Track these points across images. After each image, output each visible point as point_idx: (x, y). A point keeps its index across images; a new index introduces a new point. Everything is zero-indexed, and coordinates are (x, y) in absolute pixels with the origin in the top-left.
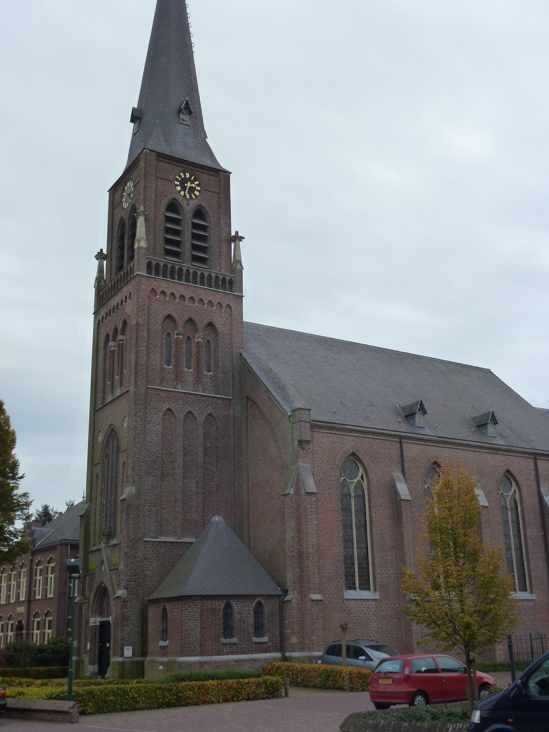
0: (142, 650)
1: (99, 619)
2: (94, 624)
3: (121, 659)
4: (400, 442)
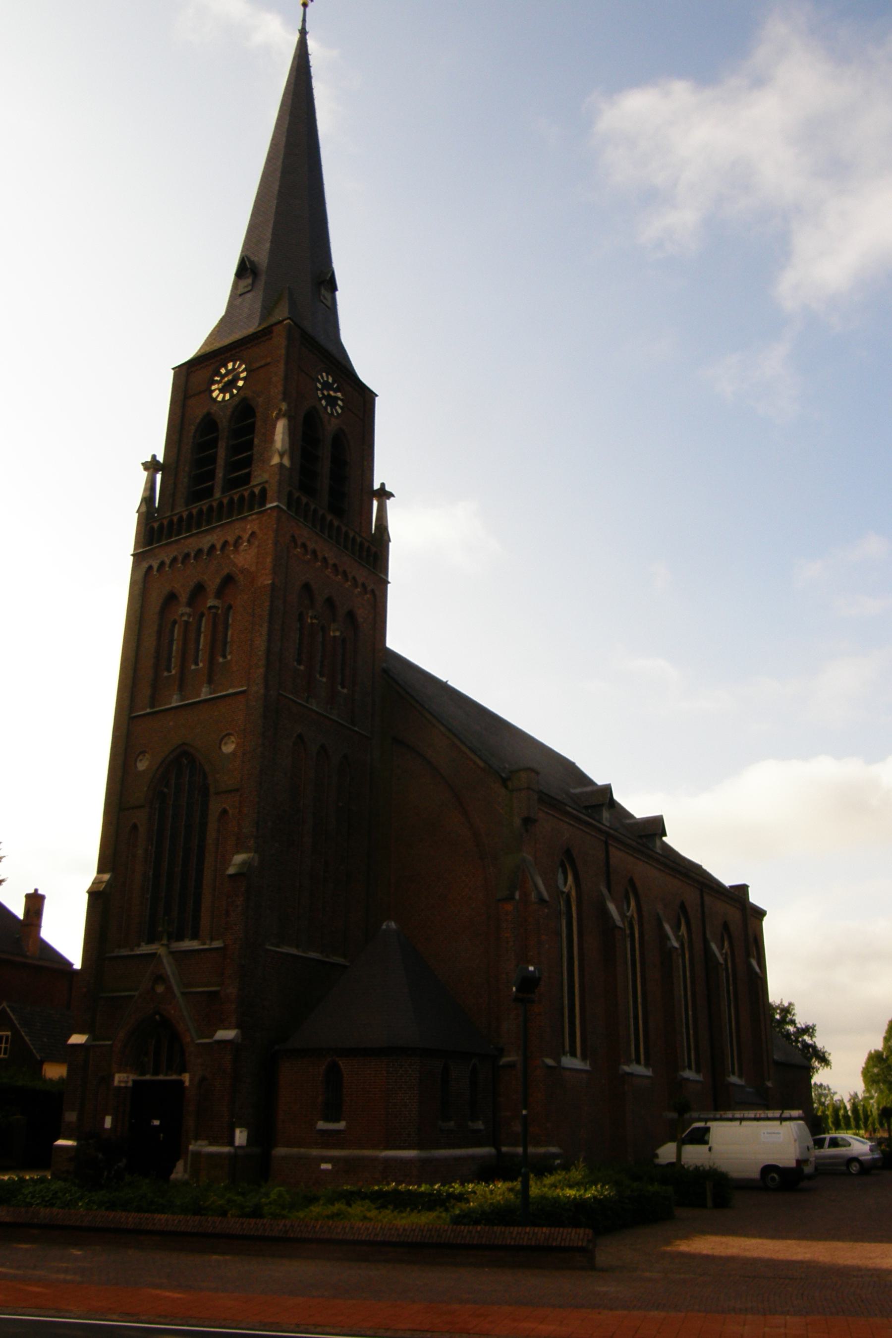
0: (264, 1137)
1: (132, 1077)
2: (123, 1085)
3: (226, 1149)
4: (607, 844)
